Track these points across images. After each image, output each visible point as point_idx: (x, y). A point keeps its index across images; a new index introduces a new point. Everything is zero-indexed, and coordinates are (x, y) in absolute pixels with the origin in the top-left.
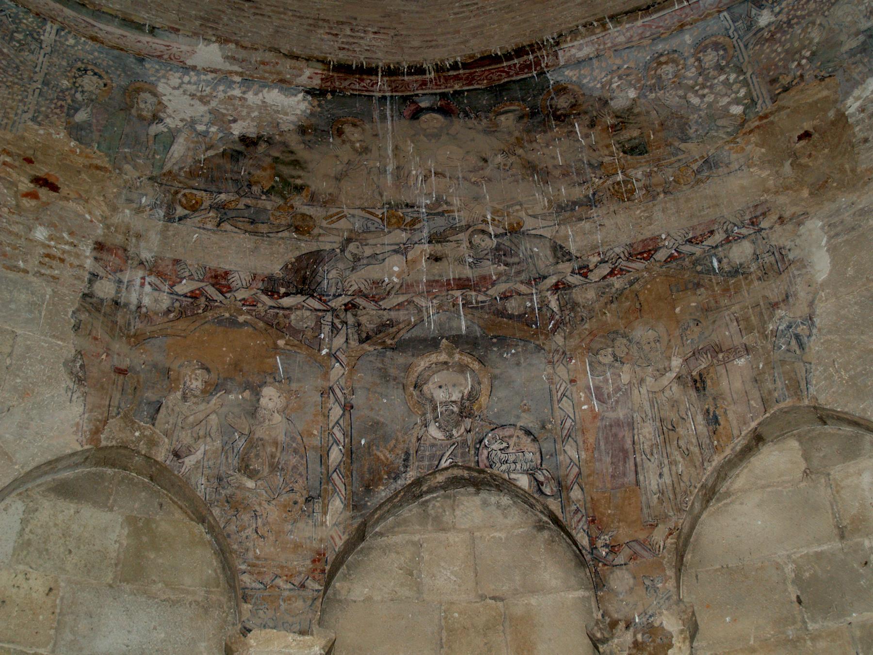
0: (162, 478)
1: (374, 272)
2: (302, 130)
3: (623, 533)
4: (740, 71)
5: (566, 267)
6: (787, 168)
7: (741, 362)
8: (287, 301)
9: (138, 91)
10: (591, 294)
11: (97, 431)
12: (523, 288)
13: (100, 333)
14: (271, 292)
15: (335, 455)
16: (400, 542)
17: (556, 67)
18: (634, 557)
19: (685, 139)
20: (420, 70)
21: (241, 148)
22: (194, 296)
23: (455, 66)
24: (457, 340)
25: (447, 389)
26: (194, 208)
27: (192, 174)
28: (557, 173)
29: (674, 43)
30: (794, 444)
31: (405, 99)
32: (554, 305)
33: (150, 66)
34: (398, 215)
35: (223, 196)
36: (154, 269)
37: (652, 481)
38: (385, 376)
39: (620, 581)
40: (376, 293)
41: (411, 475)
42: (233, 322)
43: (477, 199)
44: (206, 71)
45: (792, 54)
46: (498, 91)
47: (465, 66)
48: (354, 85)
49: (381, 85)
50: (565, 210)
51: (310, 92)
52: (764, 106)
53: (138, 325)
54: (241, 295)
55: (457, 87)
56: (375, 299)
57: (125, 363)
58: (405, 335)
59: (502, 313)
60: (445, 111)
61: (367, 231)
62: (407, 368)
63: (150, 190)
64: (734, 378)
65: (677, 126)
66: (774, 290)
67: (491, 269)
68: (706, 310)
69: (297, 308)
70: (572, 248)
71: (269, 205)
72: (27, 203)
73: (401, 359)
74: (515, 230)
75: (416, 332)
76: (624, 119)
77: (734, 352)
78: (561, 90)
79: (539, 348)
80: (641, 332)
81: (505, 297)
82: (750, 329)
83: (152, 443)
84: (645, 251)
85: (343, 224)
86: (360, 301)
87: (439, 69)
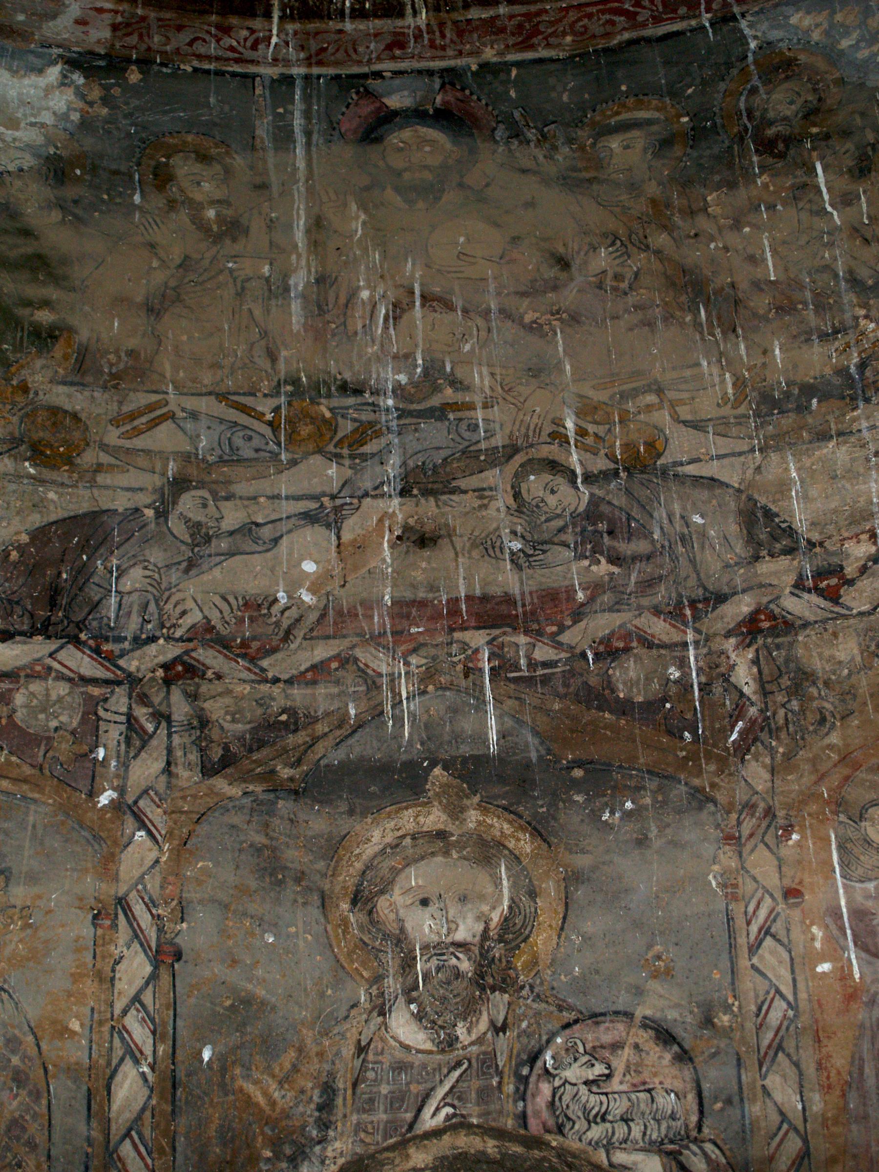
1: (247, 575)
5: (779, 571)
10: (848, 649)
12: (660, 628)
15: (129, 1090)
24: (476, 773)
25: (442, 909)
28: (762, 302)
32: (744, 676)
34: (320, 416)
38: (271, 869)
40: (252, 633)
43: (539, 371)
51: (79, 62)
56: (249, 652)
59: (599, 697)
61: (231, 458)
62: (334, 848)
67: (573, 571)
70: (799, 516)
73: (318, 822)
74: (642, 464)
75: (362, 747)
79: (701, 799)
81: (610, 651)
85: (164, 438)
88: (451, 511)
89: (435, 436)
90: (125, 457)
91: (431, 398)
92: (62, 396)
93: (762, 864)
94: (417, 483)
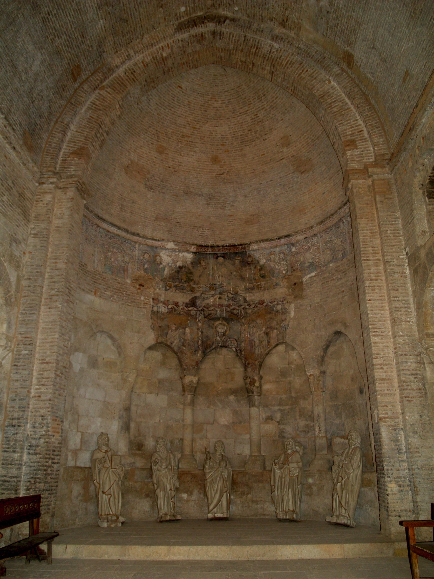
0: (169, 347)
1: (207, 301)
2: (192, 263)
3: (251, 361)
4: (287, 262)
5: (246, 304)
6: (290, 290)
7: (275, 331)
8: (190, 309)
9: (156, 256)
10: (250, 311)
11: (157, 340)
12: (237, 308)
13: (155, 319)
14: (187, 306)
15: (200, 342)
16: (212, 356)
17: (250, 251)
18: (252, 366)
19: (273, 277)
20: (219, 246)
21: (179, 270)
22: (172, 308)
23: (226, 246)
24: (224, 319)
25: (221, 329)
26: (170, 287)
27: (169, 278)
28: (247, 279)
29: (275, 250)
30: (284, 346)
31: (215, 254)
32: (243, 312)
33: (158, 249)
34: (212, 287)
35: (176, 283)
36: (164, 303)
37: (257, 352)
38: (209, 326)
39: (249, 370)
41: (214, 347)
42: (180, 314)
43: (229, 284)
44: (170, 249)
45: (297, 261)
46: (236, 253)
47: (229, 246)
48: (203, 250)
49: (209, 250)
50: (248, 290)
51: (194, 253)
52: (289, 273)
53: (162, 316)
54: (181, 307)
55: (227, 252)
56: (208, 308)
57: (160, 325)
58: (213, 317)
59: (233, 313)
60: (224, 257)
61: (206, 291)
62: (213, 324)
63: (161, 283)
64: (274, 334)
65: (272, 272)
66: (283, 317)
67: (231, 302)
68: (271, 318)
69: (192, 310)
70: (248, 299)
71: (186, 285)
72: (139, 291)
73: (212, 322)
74: (237, 293)
75: (216, 316)
76: (262, 268)
77: (275, 329)
78: (250, 256)
79: (239, 322)
80: (259, 321)
81: (233, 310)
82: (278, 324)
83: (167, 341)
84: (261, 303)
85: (201, 289)
86: (205, 309)
87: (223, 246)
88: (222, 296)
89: (221, 289)
90: (198, 291)
91: (221, 286)
92: (193, 286)
93: (243, 328)
94: (220, 293)
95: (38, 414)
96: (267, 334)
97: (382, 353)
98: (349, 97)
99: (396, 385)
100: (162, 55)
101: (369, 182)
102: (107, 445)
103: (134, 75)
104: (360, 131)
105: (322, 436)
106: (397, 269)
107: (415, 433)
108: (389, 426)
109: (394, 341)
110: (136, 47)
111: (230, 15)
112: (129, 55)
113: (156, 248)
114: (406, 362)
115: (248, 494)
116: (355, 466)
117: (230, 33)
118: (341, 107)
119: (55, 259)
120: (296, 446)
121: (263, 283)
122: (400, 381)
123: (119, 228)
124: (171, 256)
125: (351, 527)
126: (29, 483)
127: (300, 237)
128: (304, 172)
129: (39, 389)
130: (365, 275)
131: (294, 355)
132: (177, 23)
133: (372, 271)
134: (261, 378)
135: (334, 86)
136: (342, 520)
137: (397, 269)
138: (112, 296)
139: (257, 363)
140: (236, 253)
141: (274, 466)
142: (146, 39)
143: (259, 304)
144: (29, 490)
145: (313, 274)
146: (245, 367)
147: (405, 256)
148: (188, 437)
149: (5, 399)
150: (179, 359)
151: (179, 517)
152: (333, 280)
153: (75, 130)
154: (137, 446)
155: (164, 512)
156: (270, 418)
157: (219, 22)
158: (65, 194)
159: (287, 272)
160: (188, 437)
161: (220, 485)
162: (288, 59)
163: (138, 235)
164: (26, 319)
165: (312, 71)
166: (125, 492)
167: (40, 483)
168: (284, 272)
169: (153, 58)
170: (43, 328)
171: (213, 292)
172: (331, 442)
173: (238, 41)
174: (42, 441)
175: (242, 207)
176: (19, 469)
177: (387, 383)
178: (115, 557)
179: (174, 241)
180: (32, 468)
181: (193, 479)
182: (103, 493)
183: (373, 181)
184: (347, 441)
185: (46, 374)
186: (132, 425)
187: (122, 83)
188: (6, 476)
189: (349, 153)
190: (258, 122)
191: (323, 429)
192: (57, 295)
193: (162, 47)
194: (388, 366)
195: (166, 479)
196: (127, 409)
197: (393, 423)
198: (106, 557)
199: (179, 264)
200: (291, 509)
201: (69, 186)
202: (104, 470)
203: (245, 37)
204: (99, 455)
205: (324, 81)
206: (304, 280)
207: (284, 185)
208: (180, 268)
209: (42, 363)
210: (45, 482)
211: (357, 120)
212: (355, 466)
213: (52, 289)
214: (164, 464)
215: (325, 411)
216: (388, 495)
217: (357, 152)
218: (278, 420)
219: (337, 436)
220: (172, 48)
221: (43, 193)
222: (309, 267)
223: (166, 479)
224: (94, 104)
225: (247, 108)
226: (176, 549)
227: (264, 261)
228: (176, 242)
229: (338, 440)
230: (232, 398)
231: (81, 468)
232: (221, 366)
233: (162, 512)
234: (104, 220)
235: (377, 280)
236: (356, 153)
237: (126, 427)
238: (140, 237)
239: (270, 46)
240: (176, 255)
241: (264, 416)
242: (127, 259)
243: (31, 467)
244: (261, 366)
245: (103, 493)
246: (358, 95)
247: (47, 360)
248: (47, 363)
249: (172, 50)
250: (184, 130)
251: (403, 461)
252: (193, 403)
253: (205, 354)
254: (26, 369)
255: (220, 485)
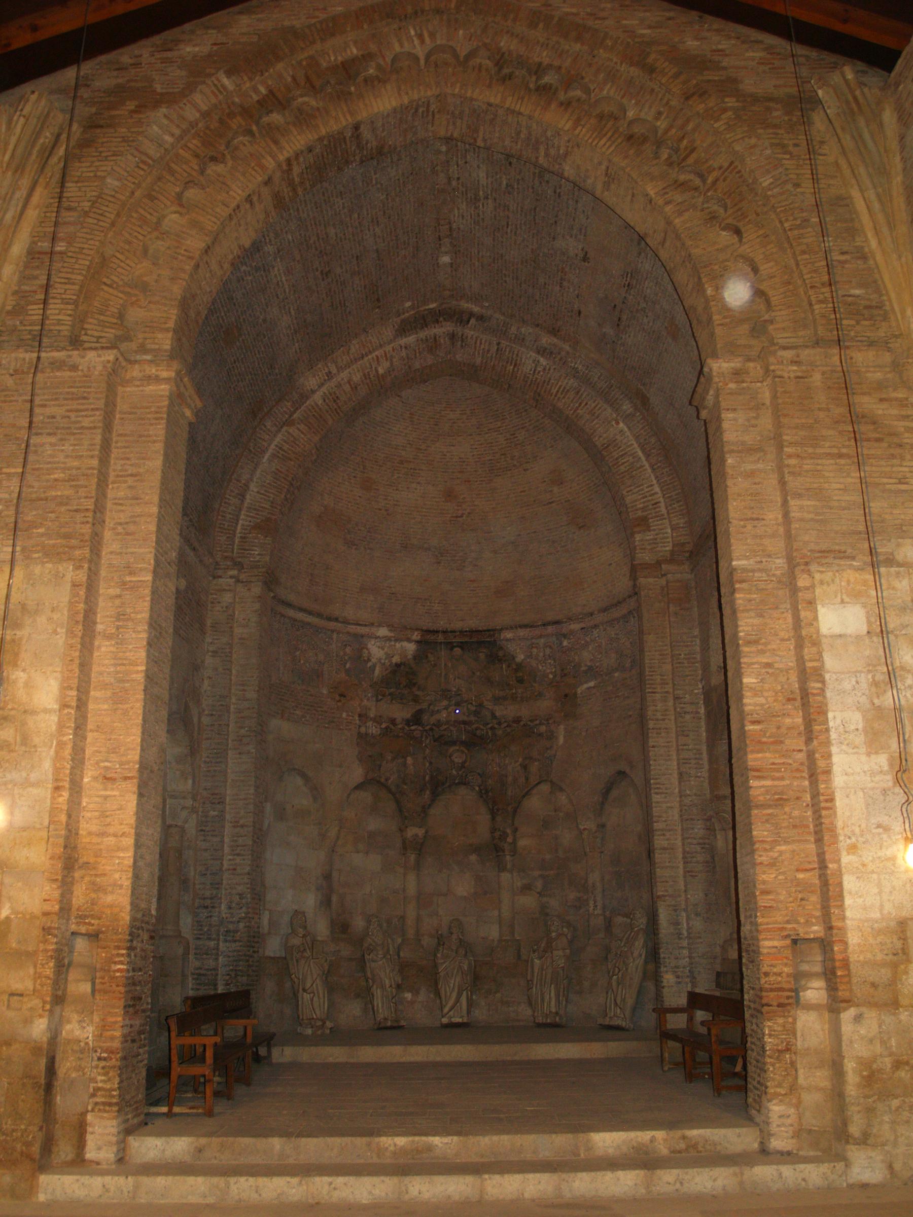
1: (437, 717)
2: (415, 658)
5: (495, 721)
6: (559, 705)
8: (413, 728)
9: (363, 648)
10: (500, 732)
14: (409, 725)
15: (427, 778)
19: (535, 681)
20: (454, 632)
22: (386, 728)
24: (463, 743)
25: (458, 759)
26: (384, 696)
36: (374, 720)
37: (509, 793)
40: (438, 724)
46: (480, 643)
48: (432, 638)
49: (440, 638)
50: (497, 700)
51: (417, 642)
52: (558, 679)
54: (400, 726)
55: (466, 640)
59: (475, 735)
60: (462, 649)
64: (534, 767)
67: (472, 718)
70: (497, 714)
72: (339, 704)
74: (481, 705)
76: (519, 667)
78: (501, 648)
81: (477, 729)
84: (517, 720)
87: (461, 632)
95: (234, 891)
96: (525, 767)
97: (664, 815)
98: (643, 451)
99: (681, 856)
100: (377, 371)
101: (663, 582)
102: (305, 927)
103: (337, 404)
104: (656, 503)
105: (598, 914)
106: (689, 708)
107: (697, 915)
108: (669, 906)
109: (680, 801)
110: (339, 360)
111: (476, 309)
112: (330, 372)
113: (362, 636)
114: (693, 829)
115: (495, 993)
116: (636, 954)
117: (477, 338)
118: (633, 463)
119: (243, 685)
120: (563, 927)
121: (520, 691)
122: (684, 852)
123: (310, 613)
124: (383, 649)
125: (627, 1030)
126: (228, 977)
127: (575, 626)
128: (582, 526)
129: (233, 860)
130: (649, 713)
131: (563, 799)
132: (398, 320)
133: (658, 708)
134: (516, 830)
135: (620, 432)
136: (617, 1022)
137: (689, 708)
138: (303, 716)
139: (509, 808)
140: (480, 643)
141: (532, 955)
142: (355, 347)
143: (514, 722)
144: (228, 985)
145: (592, 684)
146: (493, 814)
147: (701, 691)
148: (411, 913)
149: (192, 874)
150: (398, 802)
151: (403, 1023)
152: (618, 697)
153: (256, 490)
154: (341, 928)
155: (382, 1016)
156: (527, 888)
157: (461, 322)
158: (249, 589)
159: (555, 677)
160: (411, 913)
161: (457, 980)
162: (560, 383)
163: (336, 620)
164: (212, 769)
165: (593, 405)
166: (331, 989)
167: (242, 976)
168: (551, 676)
169: (364, 375)
170: (233, 780)
171: (445, 703)
172: (610, 922)
173: (488, 351)
174: (241, 925)
175: (491, 568)
176: (217, 959)
177: (669, 854)
178: (342, 1060)
179: (388, 626)
180: (231, 959)
181: (421, 973)
182: (304, 990)
183: (667, 582)
184: (629, 921)
185: (240, 841)
186: (334, 899)
187: (321, 417)
188: (201, 969)
189: (638, 537)
190: (516, 445)
191: (599, 904)
192: (249, 736)
193: (377, 357)
194: (671, 833)
195: (383, 972)
196: (328, 877)
197: (673, 903)
198: (331, 1060)
199: (396, 659)
200: (554, 1010)
201: (253, 579)
202: (303, 961)
203: (498, 344)
204: (296, 941)
205: (609, 422)
206: (579, 691)
207: (554, 542)
208: (398, 665)
209: (234, 827)
210: (248, 975)
211: (652, 485)
212: (636, 954)
213: (241, 728)
214: (380, 953)
215: (603, 879)
216: (663, 987)
217: (649, 536)
218: (538, 890)
219: (619, 914)
220: (391, 360)
221: (219, 590)
222: (586, 672)
223: (383, 972)
224: (280, 448)
225: (499, 424)
226: (413, 1049)
227: (523, 657)
228: (391, 627)
229: (619, 920)
230: (473, 858)
231: (271, 958)
232: (458, 810)
233: (380, 1017)
234: (289, 605)
235: (664, 720)
236: (648, 538)
237: (326, 902)
238: (340, 622)
239: (534, 361)
240: (391, 646)
241: (519, 884)
242: (321, 657)
243: (229, 957)
244: (515, 812)
245: (304, 990)
246: (654, 448)
247: (241, 822)
248: (242, 826)
249: (392, 364)
250: (403, 453)
251: (683, 948)
252: (418, 866)
253: (435, 795)
254: (216, 836)
255: (457, 980)
